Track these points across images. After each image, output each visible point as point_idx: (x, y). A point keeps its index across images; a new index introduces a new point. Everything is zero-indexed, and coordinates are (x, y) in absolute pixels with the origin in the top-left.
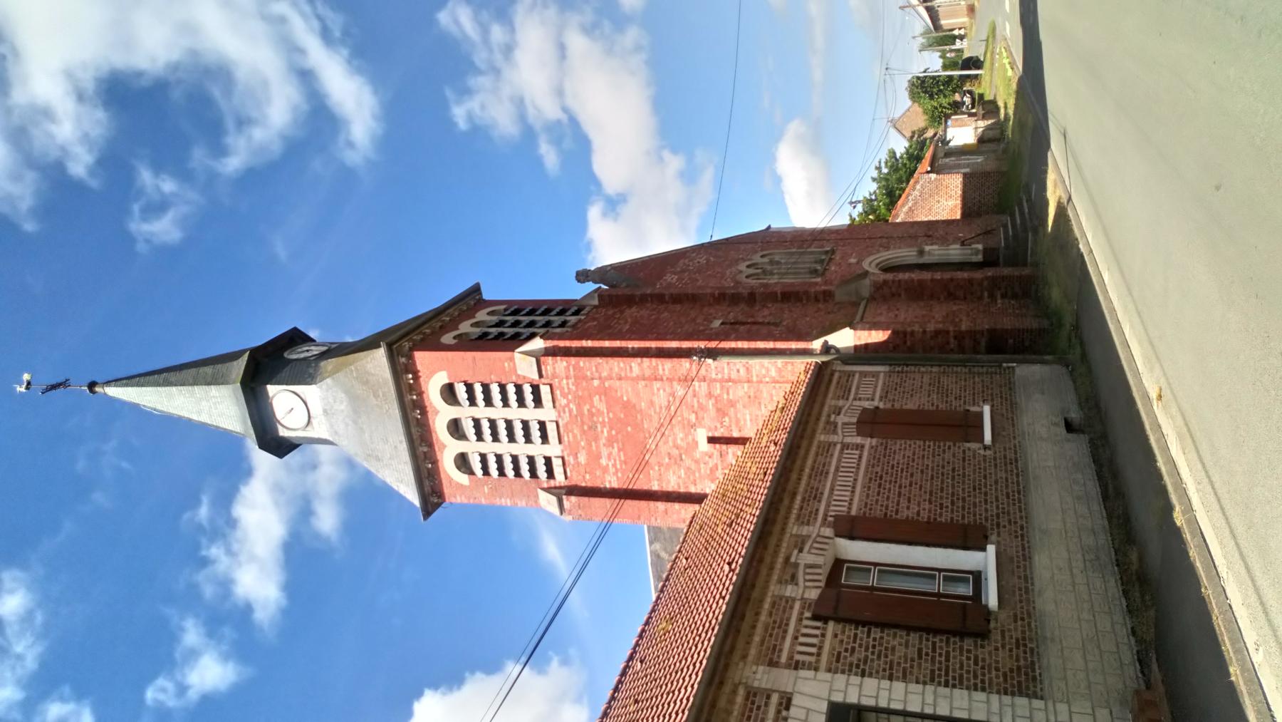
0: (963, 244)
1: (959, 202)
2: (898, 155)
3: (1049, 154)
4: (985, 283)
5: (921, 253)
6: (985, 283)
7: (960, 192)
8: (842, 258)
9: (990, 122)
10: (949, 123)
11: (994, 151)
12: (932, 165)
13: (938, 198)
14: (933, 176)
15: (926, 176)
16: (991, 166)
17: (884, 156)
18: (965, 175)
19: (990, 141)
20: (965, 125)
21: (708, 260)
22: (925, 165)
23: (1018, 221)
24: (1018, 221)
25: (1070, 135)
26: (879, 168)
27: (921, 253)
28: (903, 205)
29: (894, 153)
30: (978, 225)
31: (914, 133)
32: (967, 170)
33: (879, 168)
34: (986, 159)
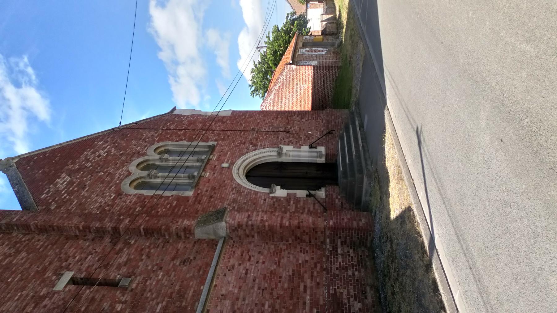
0: (311, 147)
1: (310, 85)
2: (280, 28)
3: (386, 113)
4: (328, 233)
5: (280, 154)
6: (328, 233)
7: (311, 79)
8: (218, 159)
9: (332, 16)
10: (309, 5)
11: (333, 45)
12: (293, 59)
13: (296, 91)
14: (294, 67)
15: (289, 66)
16: (330, 60)
17: (271, 29)
18: (314, 67)
19: (331, 34)
20: (317, 8)
21: (109, 152)
22: (288, 56)
23: (354, 153)
24: (354, 153)
25: (425, 136)
26: (268, 37)
27: (280, 154)
28: (275, 85)
29: (278, 27)
30: (323, 114)
31: (288, 14)
32: (315, 63)
33: (268, 37)
34: (328, 53)
